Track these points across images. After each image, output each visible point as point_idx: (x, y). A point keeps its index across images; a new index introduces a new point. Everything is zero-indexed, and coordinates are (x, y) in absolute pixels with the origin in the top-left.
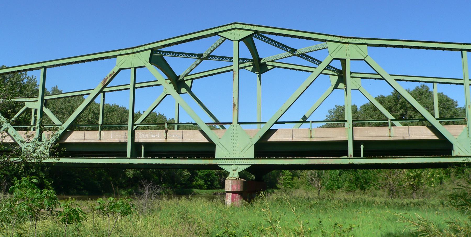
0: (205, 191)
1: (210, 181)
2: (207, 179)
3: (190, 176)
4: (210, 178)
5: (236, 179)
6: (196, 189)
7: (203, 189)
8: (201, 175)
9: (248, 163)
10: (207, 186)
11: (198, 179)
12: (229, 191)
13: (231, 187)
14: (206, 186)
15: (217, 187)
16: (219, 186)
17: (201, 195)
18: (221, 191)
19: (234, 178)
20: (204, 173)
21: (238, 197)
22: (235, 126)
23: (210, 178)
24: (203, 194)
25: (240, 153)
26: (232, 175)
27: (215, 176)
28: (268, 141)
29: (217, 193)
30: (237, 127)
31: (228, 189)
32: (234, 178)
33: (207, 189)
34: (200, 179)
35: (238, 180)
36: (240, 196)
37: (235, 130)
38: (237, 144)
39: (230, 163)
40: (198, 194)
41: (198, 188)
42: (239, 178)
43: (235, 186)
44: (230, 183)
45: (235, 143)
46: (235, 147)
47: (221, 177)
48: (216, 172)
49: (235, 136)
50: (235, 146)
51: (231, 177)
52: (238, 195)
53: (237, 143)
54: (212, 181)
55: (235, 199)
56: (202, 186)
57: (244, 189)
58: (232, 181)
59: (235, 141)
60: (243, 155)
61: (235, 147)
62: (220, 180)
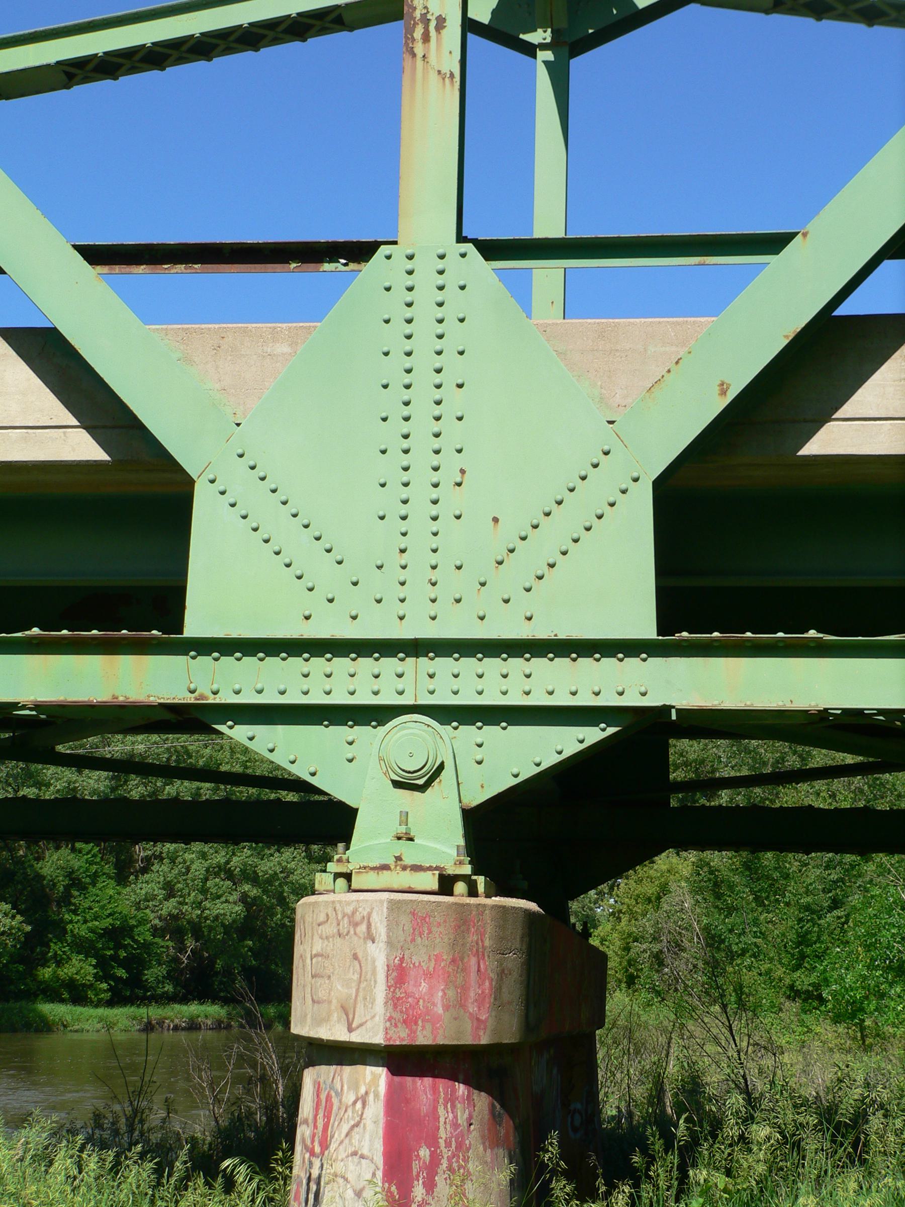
0: (101, 1011)
1: (122, 964)
2: (109, 953)
3: (27, 935)
4: (125, 947)
5: (446, 884)
6: (52, 1001)
7: (92, 1002)
8: (82, 931)
9: (585, 700)
10: (111, 989)
11: (64, 952)
12: (356, 1038)
13: (380, 992)
14: (104, 986)
15: (159, 991)
16: (169, 988)
17: (76, 1031)
18: (180, 1012)
19: (417, 868)
20: (97, 923)
21: (462, 1118)
22: (425, 267)
23: (125, 947)
24: (87, 1027)
25: (500, 563)
26: (388, 839)
27: (154, 936)
28: (800, 453)
29: (161, 1023)
30: (451, 280)
31: (347, 1012)
32: (417, 868)
33: (110, 1004)
34: (79, 953)
35: (473, 901)
36: (482, 1100)
37: (425, 312)
38: (448, 476)
39: (364, 698)
40: (65, 1026)
41: (66, 996)
42: (481, 880)
43: (428, 975)
44: (371, 937)
45: (422, 459)
46: (420, 509)
47: (182, 942)
48: (157, 921)
49: (423, 378)
50: (420, 493)
51: (385, 867)
52: (461, 1089)
53: (451, 463)
54: (136, 964)
55: (433, 1142)
56: (84, 985)
57: (528, 1026)
58: (394, 906)
59: (422, 443)
60: (523, 604)
61: (420, 509)
62: (176, 960)
